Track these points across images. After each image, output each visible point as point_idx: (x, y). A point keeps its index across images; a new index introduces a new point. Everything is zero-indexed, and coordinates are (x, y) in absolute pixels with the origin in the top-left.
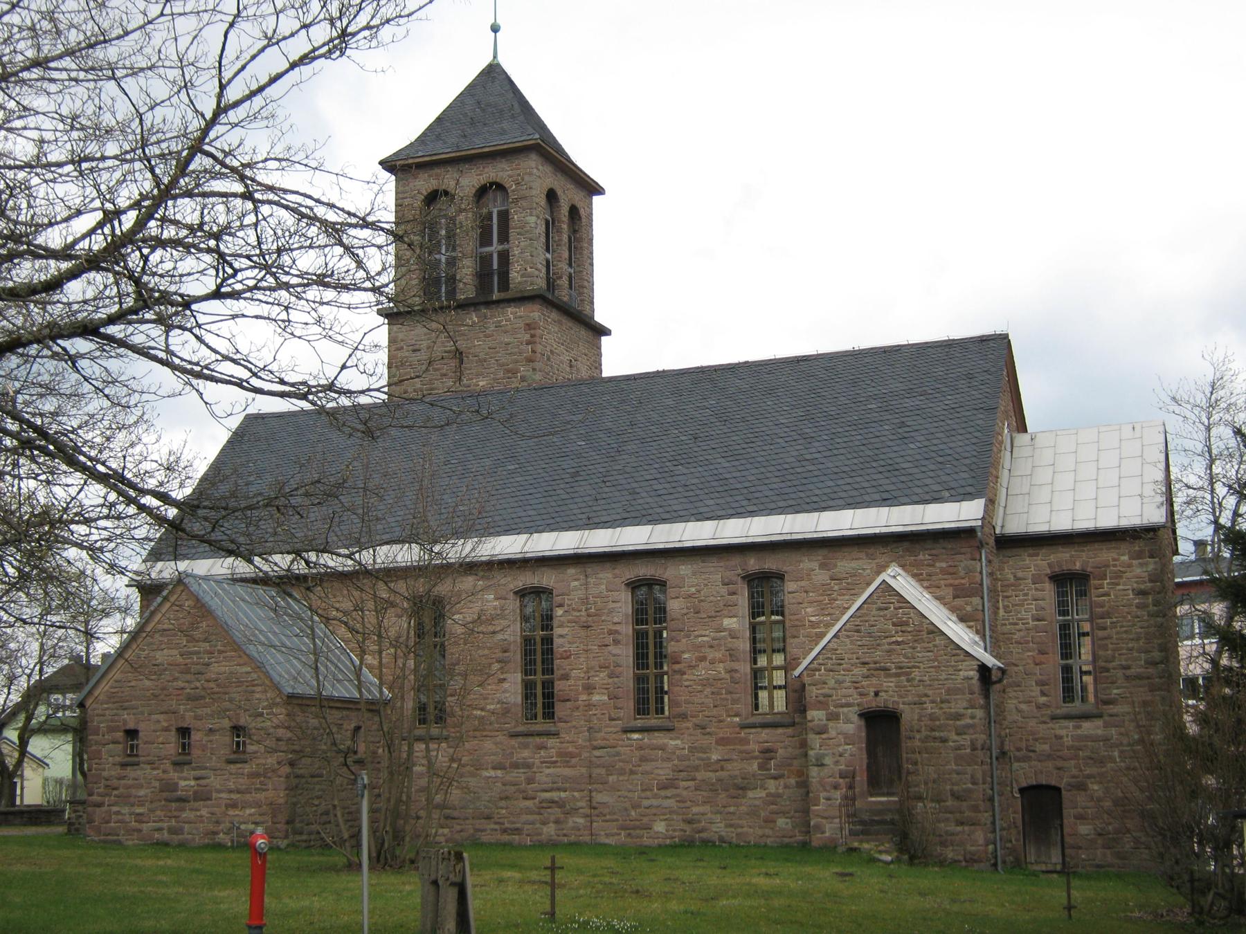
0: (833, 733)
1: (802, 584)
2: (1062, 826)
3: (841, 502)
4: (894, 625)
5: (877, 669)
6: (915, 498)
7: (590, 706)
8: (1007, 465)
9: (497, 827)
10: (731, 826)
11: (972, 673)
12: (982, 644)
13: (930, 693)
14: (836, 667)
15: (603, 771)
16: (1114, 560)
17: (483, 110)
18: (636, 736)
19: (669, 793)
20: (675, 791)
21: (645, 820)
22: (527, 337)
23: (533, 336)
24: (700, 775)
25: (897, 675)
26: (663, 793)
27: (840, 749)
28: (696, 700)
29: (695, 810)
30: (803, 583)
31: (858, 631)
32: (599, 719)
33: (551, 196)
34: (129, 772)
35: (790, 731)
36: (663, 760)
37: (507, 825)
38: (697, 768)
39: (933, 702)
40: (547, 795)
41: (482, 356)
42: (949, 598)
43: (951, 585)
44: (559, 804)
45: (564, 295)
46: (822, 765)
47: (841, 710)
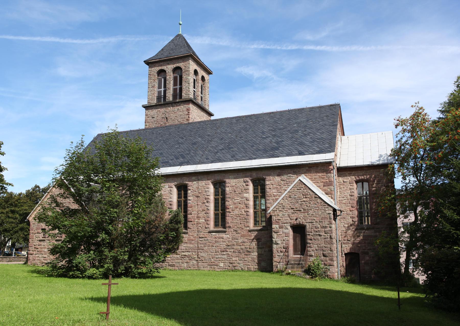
0: (281, 233)
1: (272, 182)
2: (359, 267)
3: (285, 154)
4: (303, 195)
5: (297, 211)
6: (310, 153)
7: (198, 223)
8: (340, 145)
9: (167, 264)
10: (246, 265)
11: (330, 212)
12: (334, 202)
13: (315, 219)
14: (282, 210)
15: (203, 245)
16: (378, 175)
17: (176, 46)
18: (214, 234)
19: (225, 253)
20: (227, 253)
21: (216, 263)
22: (187, 113)
23: (188, 112)
24: (235, 247)
25: (304, 213)
26: (223, 253)
27: (284, 238)
28: (234, 221)
29: (234, 259)
30: (271, 182)
31: (290, 197)
32: (202, 228)
33: (196, 72)
34: (42, 243)
35: (266, 232)
36: (223, 242)
37: (170, 263)
38: (234, 245)
39: (316, 222)
40: (184, 253)
41: (173, 119)
42: (322, 187)
43: (323, 182)
44: (188, 256)
45: (199, 102)
46: (277, 244)
47: (284, 225)
